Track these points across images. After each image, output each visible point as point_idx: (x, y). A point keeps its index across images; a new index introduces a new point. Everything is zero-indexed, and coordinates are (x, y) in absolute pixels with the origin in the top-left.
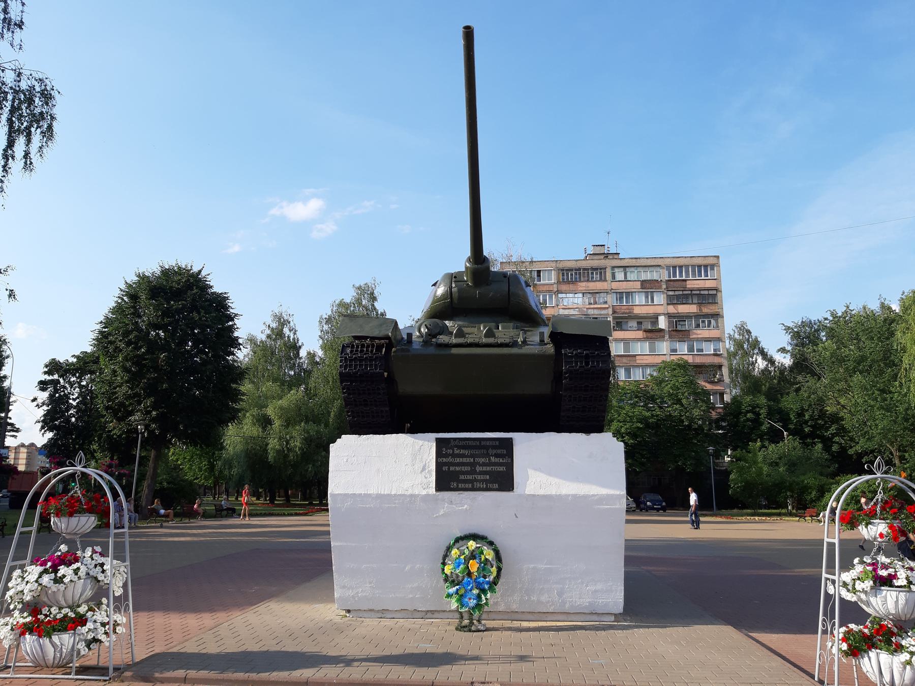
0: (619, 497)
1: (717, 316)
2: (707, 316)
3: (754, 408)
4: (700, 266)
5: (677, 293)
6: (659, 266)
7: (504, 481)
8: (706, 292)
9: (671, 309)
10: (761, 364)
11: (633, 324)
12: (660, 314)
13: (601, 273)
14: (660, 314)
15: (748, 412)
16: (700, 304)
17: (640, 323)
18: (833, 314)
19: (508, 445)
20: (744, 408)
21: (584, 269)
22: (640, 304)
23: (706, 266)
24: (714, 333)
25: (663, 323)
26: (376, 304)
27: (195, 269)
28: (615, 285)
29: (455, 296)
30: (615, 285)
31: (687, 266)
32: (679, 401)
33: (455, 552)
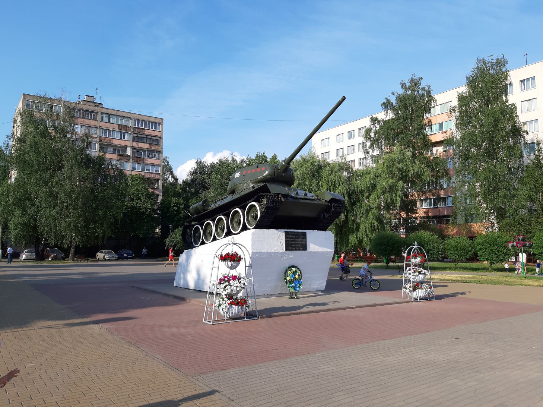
0: (329, 253)
1: (159, 152)
3: (177, 205)
4: (152, 123)
5: (139, 135)
6: (130, 118)
7: (304, 247)
8: (155, 138)
9: (135, 144)
10: (171, 180)
11: (111, 149)
12: (128, 146)
13: (94, 115)
14: (128, 146)
15: (174, 206)
16: (151, 144)
17: (114, 150)
18: (275, 157)
19: (305, 234)
20: (173, 204)
21: (83, 110)
22: (116, 139)
23: (156, 123)
25: (129, 152)
28: (102, 124)
29: (276, 175)
30: (102, 124)
31: (146, 121)
32: (139, 198)
33: (289, 272)
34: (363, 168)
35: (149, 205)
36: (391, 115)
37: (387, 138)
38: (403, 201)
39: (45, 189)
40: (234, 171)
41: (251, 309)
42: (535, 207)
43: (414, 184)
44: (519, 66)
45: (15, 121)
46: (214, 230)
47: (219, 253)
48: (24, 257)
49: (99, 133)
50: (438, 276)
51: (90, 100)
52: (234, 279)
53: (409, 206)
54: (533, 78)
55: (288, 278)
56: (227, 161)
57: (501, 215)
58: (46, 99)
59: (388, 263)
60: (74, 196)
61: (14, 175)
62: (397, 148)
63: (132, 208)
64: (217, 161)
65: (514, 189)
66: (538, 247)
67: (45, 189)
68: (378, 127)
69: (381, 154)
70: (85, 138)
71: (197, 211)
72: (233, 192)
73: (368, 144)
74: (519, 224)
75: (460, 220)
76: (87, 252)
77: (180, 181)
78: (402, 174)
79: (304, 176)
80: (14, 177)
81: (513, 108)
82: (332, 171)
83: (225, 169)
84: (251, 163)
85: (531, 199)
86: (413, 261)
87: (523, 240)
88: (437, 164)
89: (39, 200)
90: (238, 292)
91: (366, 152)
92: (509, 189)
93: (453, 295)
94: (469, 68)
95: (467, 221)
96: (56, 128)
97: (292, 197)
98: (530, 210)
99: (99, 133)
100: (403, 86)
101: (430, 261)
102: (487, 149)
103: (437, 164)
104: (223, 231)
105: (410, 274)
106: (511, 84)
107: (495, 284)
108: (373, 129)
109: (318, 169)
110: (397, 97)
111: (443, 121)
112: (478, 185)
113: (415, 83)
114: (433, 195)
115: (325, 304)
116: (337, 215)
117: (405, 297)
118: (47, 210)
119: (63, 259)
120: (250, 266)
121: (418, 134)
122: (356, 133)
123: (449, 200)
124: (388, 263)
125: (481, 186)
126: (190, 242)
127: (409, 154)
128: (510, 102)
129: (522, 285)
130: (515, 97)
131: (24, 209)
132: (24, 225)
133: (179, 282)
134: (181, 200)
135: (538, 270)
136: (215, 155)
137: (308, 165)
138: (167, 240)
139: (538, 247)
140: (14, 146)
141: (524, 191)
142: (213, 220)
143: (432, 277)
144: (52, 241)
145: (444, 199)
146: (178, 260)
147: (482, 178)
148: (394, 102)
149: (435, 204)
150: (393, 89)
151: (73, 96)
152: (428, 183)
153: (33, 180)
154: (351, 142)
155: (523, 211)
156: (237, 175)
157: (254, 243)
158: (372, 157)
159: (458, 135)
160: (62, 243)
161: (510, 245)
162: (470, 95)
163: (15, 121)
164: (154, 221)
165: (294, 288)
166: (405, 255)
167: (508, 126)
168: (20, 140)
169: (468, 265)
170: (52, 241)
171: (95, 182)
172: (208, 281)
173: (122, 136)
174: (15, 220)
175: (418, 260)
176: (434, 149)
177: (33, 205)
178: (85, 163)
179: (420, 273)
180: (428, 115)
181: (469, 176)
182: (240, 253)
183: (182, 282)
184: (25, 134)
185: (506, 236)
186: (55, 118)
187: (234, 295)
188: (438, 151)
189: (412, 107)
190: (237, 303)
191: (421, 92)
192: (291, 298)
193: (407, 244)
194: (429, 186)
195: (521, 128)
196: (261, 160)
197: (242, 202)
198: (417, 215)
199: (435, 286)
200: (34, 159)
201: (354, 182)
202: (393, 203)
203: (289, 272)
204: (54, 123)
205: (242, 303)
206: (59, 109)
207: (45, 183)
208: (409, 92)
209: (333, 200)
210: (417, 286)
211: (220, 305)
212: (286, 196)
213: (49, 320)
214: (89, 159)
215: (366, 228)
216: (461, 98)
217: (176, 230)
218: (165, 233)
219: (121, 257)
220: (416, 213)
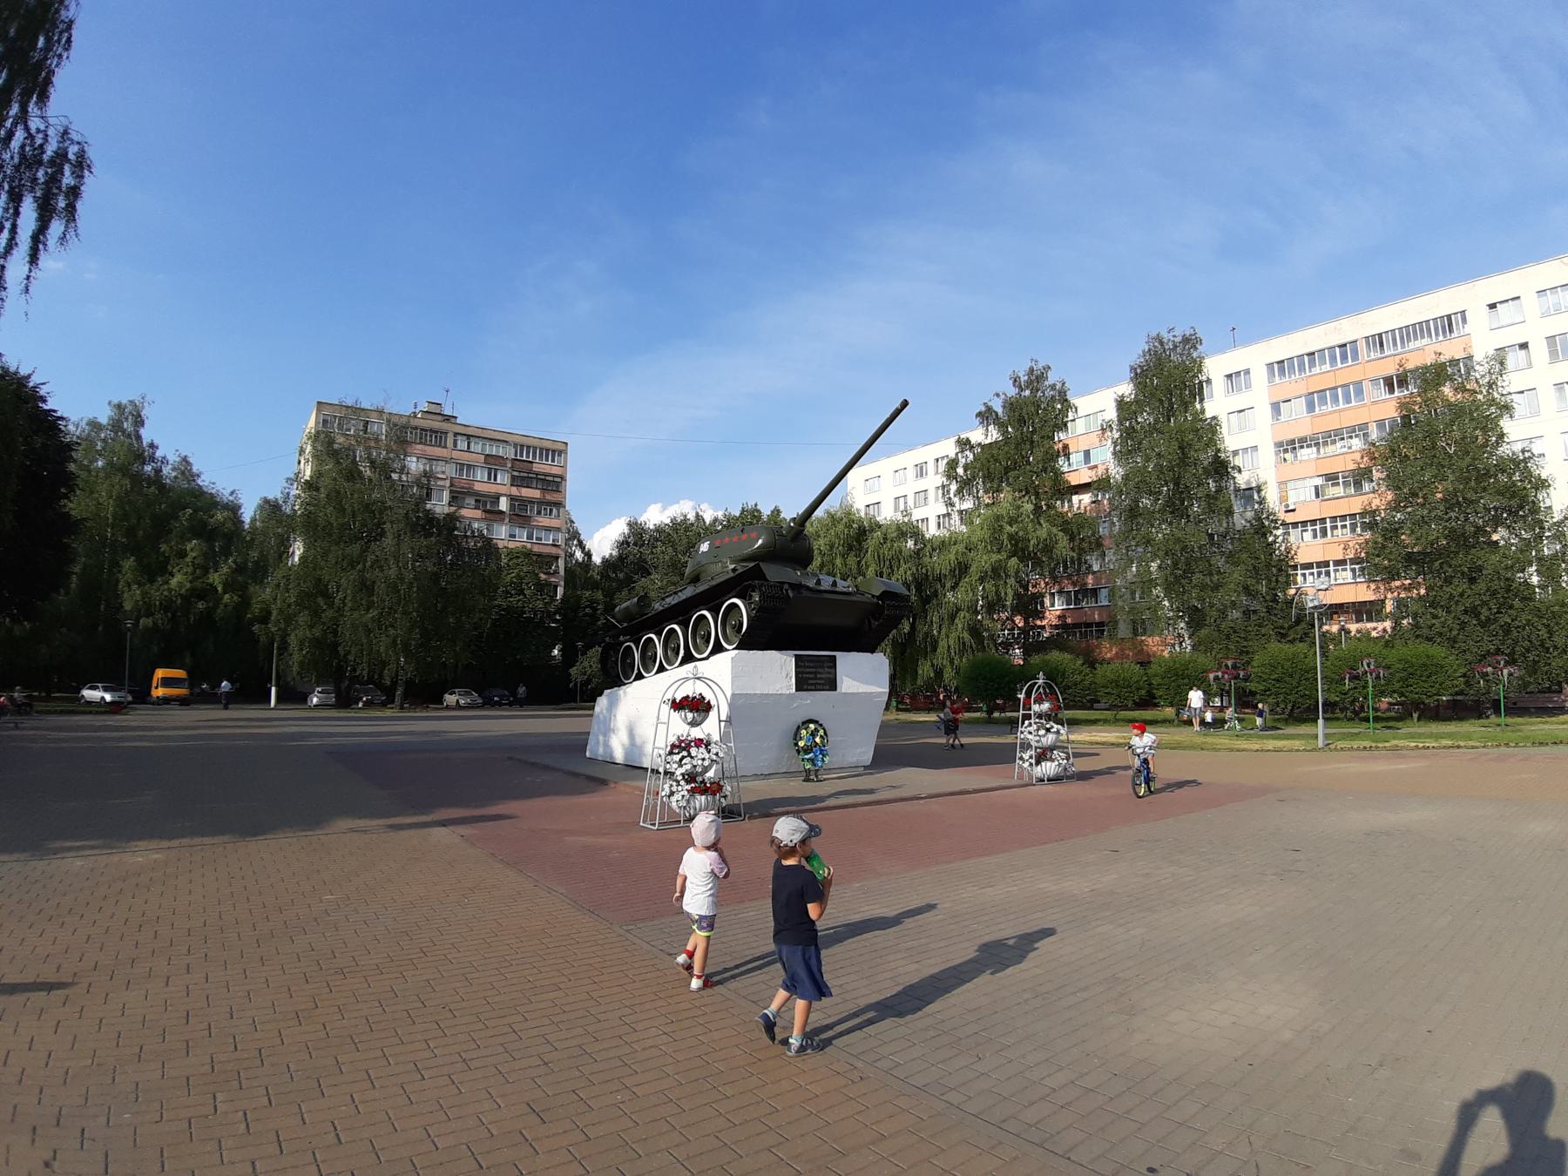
1: (559, 505)
2: (549, 503)
7: (832, 685)
9: (514, 491)
11: (471, 501)
18: (777, 512)
20: (584, 602)
22: (480, 481)
24: (555, 523)
25: (504, 505)
26: (142, 431)
27: (23, 372)
28: (455, 454)
32: (521, 592)
33: (804, 732)
34: (943, 533)
35: (540, 605)
36: (994, 435)
37: (988, 477)
38: (1017, 595)
39: (353, 575)
40: (700, 538)
41: (729, 801)
42: (1255, 605)
43: (1038, 563)
44: (1222, 350)
45: (302, 451)
46: (660, 651)
47: (669, 696)
48: (315, 700)
49: (450, 471)
50: (1082, 736)
51: (435, 412)
52: (698, 746)
53: (1030, 606)
54: (1247, 372)
55: (801, 744)
56: (686, 519)
57: (1196, 619)
58: (357, 410)
59: (990, 712)
60: (402, 588)
61: (298, 550)
62: (1006, 496)
63: (509, 609)
64: (668, 521)
65: (1219, 573)
66: (1260, 679)
67: (353, 575)
68: (971, 457)
69: (977, 508)
70: (424, 481)
71: (628, 615)
72: (695, 579)
73: (954, 487)
74: (1228, 637)
75: (1124, 630)
76: (425, 694)
77: (597, 559)
78: (1016, 545)
79: (832, 547)
80: (298, 553)
81: (1213, 426)
82: (885, 539)
83: (683, 534)
84: (731, 524)
85: (1246, 589)
86: (1036, 708)
87: (1235, 667)
88: (1081, 527)
89: (341, 595)
90: (706, 769)
91: (950, 504)
92: (1211, 574)
93: (1109, 771)
94: (1135, 352)
95: (1135, 633)
96: (372, 462)
97: (808, 588)
98: (1247, 613)
99: (450, 471)
100: (1016, 381)
101: (1067, 707)
102: (1169, 502)
103: (1081, 527)
104: (678, 654)
105: (1030, 733)
106: (1209, 381)
107: (1184, 748)
108: (962, 461)
109: (858, 534)
110: (1005, 402)
111: (1090, 444)
112: (1154, 566)
113: (1036, 378)
114: (1074, 584)
115: (871, 791)
116: (895, 622)
117: (1021, 777)
118: (356, 614)
119: (384, 705)
120: (729, 721)
121: (1045, 470)
122: (931, 467)
123: (1104, 592)
124: (990, 712)
125: (1160, 567)
126: (617, 673)
127: (1029, 507)
128: (1208, 415)
129: (1232, 750)
130: (1216, 404)
131: (316, 613)
132: (317, 643)
133: (594, 749)
134: (599, 595)
135: (1259, 721)
136: (664, 509)
137: (841, 527)
138: (573, 671)
139: (1260, 679)
140: (298, 497)
141: (1237, 575)
142: (659, 634)
143: (1072, 737)
144: (363, 671)
145: (1094, 593)
146: (593, 708)
147: (1161, 553)
148: (1000, 410)
149: (1077, 601)
150: (998, 388)
151: (405, 403)
152: (1065, 562)
153: (332, 558)
154: (921, 484)
155: (1235, 614)
156: (704, 547)
157: (735, 678)
158: (961, 512)
159: (1116, 472)
160: (381, 675)
161: (1212, 676)
162: (1136, 401)
163: (302, 451)
164: (565, 631)
165: (812, 760)
166: (1022, 696)
167: (1206, 458)
168: (310, 486)
169: (1136, 714)
170: (363, 671)
171: (441, 561)
172: (648, 748)
173: (492, 475)
174: (300, 633)
175: (1046, 706)
176: (1075, 498)
177: (331, 606)
178: (423, 527)
179: (1048, 730)
180: (1062, 436)
181: (1140, 549)
182: (709, 696)
183: (601, 750)
184: (318, 474)
185: (1202, 659)
186: (372, 444)
187: (697, 774)
188: (1083, 500)
189: (1032, 420)
190: (703, 789)
191: (1049, 393)
192: (807, 780)
193: (1025, 675)
194: (1065, 567)
195: (1229, 462)
196: (750, 518)
197: (712, 599)
198: (1044, 622)
199: (1076, 755)
200: (332, 520)
201: (926, 560)
202: (999, 599)
203: (804, 732)
204: (370, 454)
205: (713, 789)
206: (380, 428)
207: (352, 565)
208: (1027, 393)
209: (886, 595)
210: (1043, 756)
211: (672, 793)
212: (797, 587)
213: (365, 817)
214: (430, 518)
215: (1085, 989)
216: (1121, 404)
217: (590, 653)
218: (570, 657)
219: (488, 703)
220: (1043, 618)
